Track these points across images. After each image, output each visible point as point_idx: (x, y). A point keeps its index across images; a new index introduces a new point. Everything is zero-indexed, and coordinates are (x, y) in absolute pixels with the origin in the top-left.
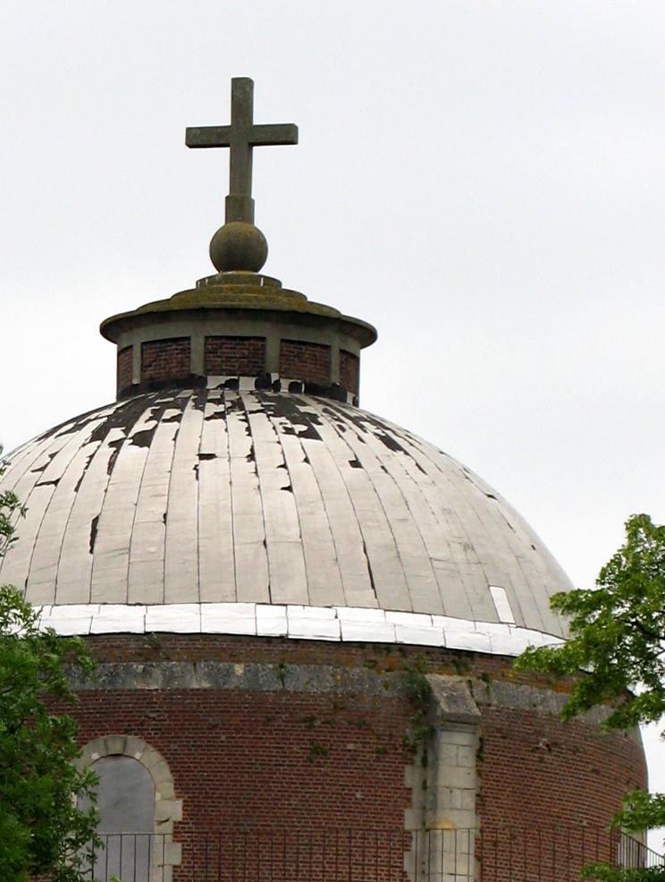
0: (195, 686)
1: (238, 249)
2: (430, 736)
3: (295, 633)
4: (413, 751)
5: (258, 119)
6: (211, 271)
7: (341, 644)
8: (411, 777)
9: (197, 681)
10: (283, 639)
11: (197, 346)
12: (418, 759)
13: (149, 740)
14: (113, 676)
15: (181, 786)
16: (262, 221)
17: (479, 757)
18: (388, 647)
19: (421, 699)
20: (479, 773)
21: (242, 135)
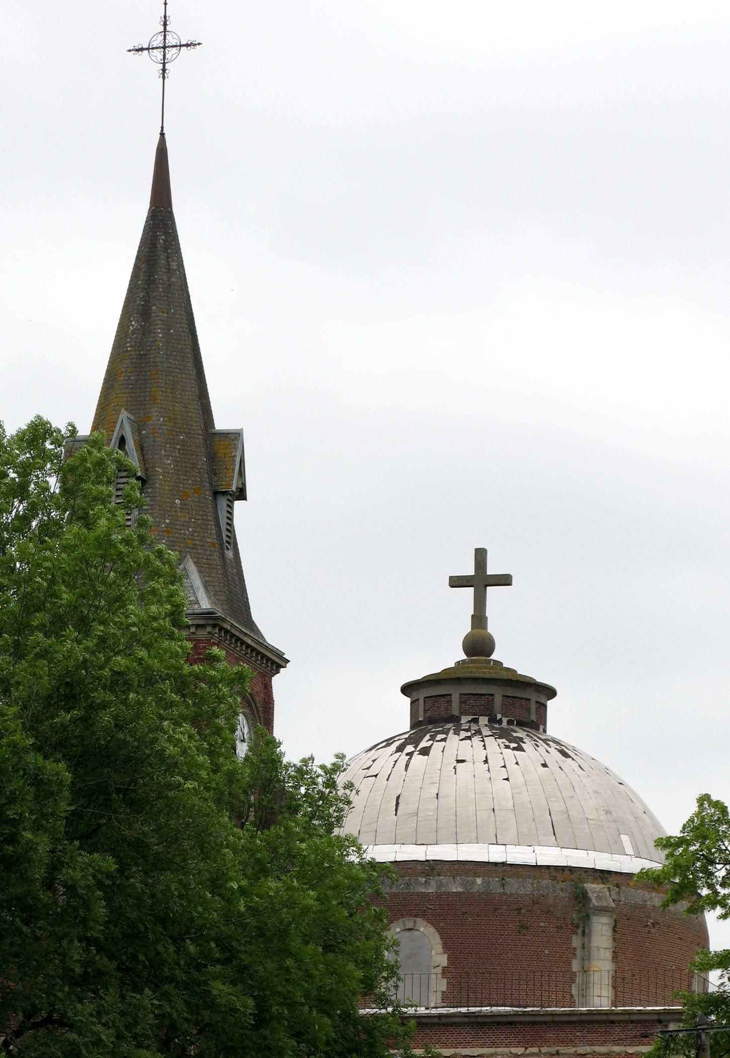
0: (454, 890)
1: (479, 645)
2: (587, 917)
3: (510, 861)
4: (577, 927)
5: (490, 572)
6: (463, 657)
7: (537, 867)
8: (576, 942)
9: (456, 888)
10: (503, 864)
11: (455, 698)
12: (580, 931)
13: (428, 921)
14: (408, 885)
15: (446, 947)
16: (492, 628)
17: (614, 930)
18: (563, 868)
19: (582, 898)
20: (614, 939)
21: (480, 580)
